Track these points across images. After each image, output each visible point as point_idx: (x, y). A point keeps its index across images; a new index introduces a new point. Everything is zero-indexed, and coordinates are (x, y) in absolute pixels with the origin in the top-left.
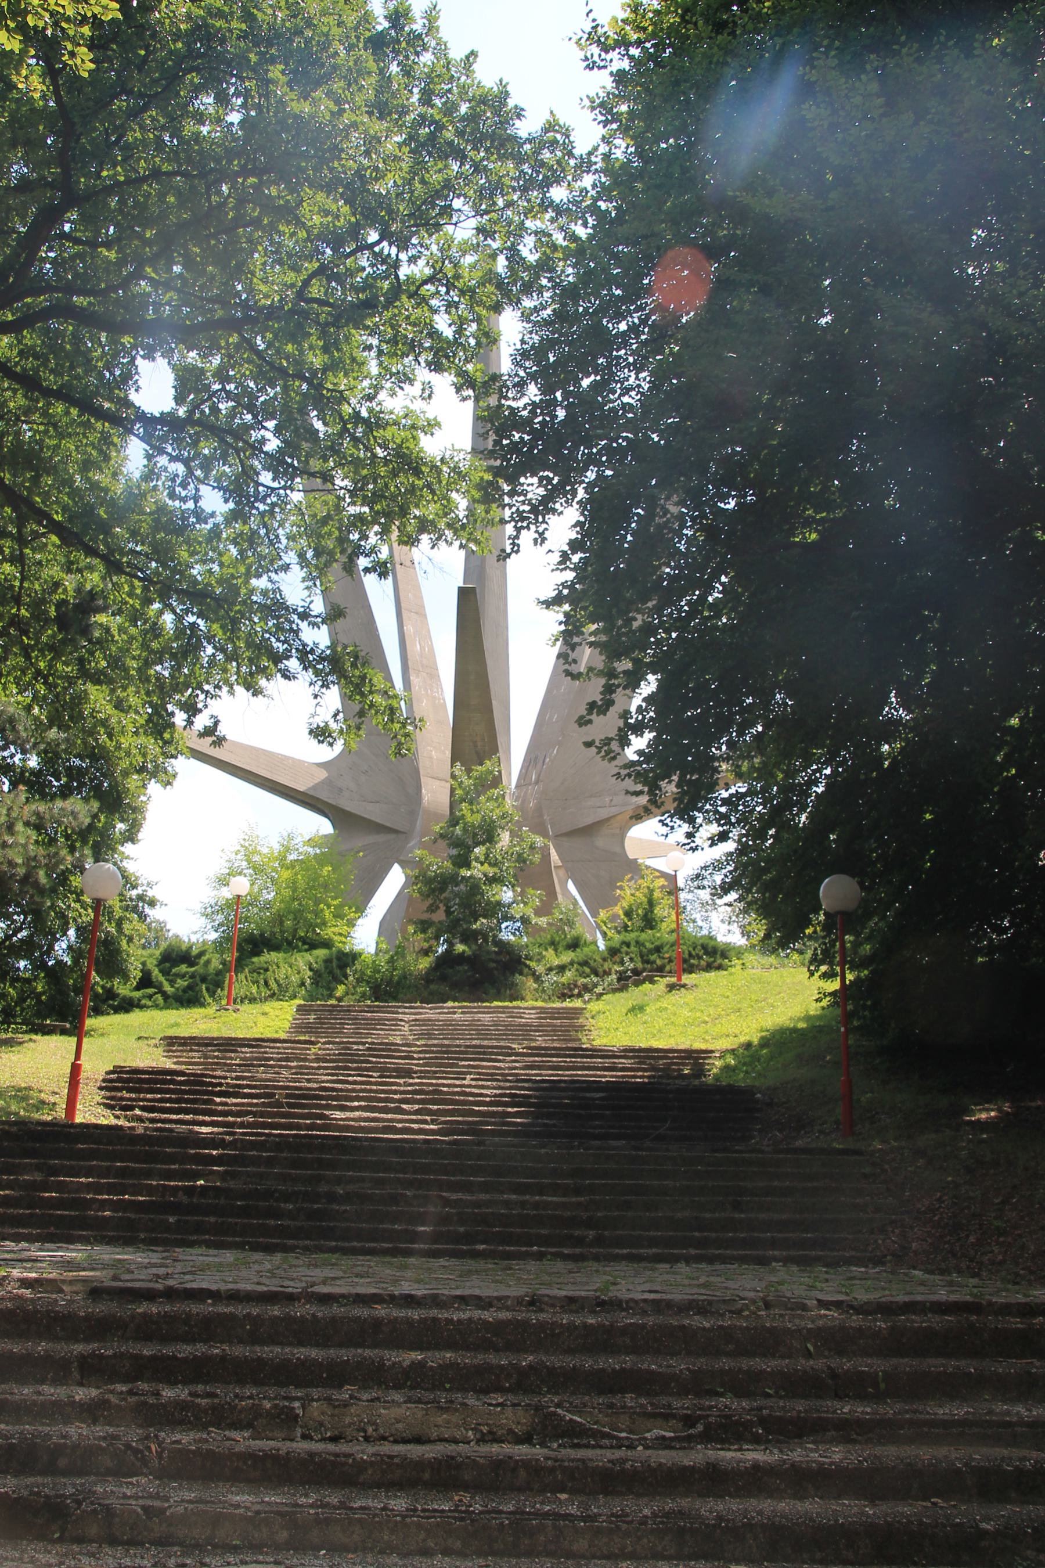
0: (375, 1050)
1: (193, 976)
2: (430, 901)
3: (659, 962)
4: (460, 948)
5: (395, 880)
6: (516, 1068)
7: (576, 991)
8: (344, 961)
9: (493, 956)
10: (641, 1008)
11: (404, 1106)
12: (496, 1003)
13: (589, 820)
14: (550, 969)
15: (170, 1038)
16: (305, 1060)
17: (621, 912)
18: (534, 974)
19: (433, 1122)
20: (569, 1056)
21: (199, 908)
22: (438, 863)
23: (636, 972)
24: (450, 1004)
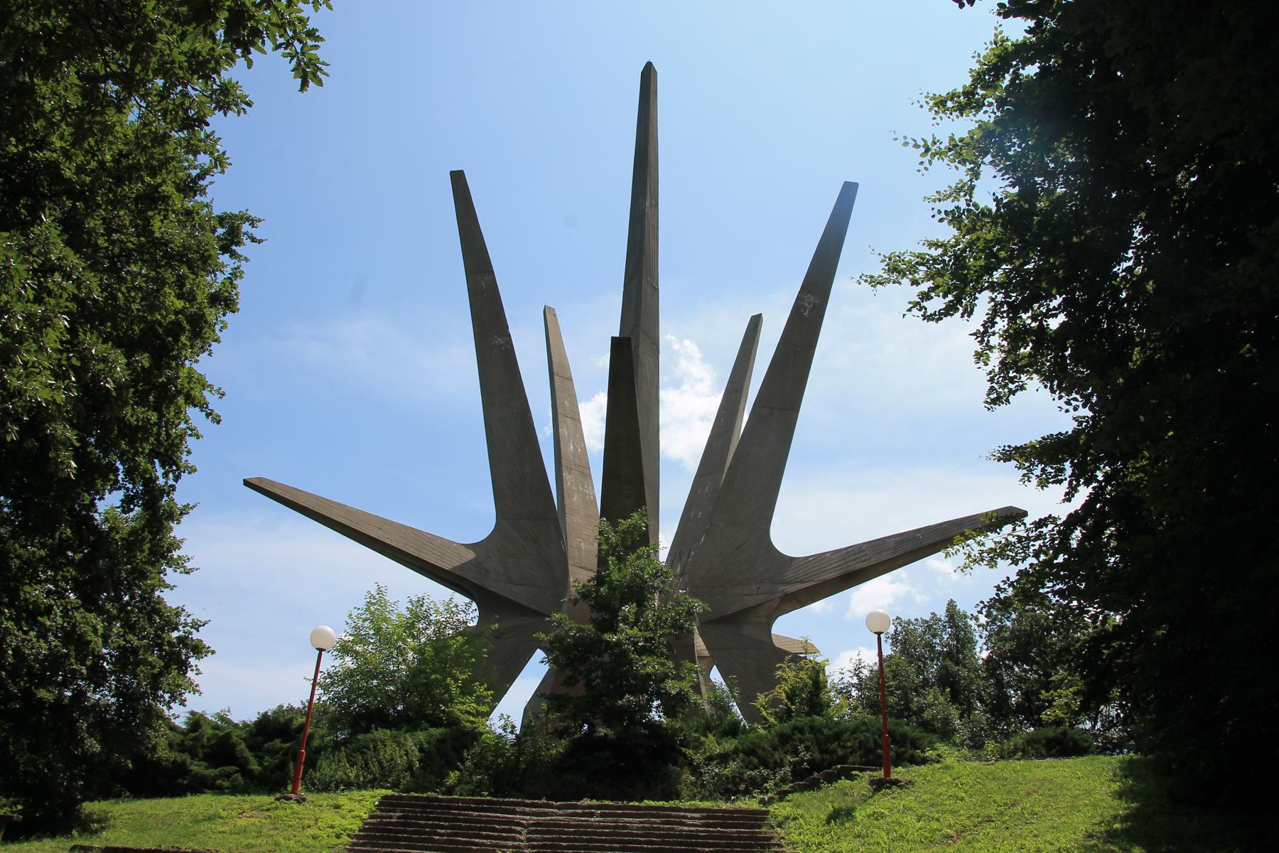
2: (568, 673)
3: (840, 752)
4: (602, 731)
7: (742, 787)
8: (460, 740)
10: (848, 813)
12: (647, 802)
13: (736, 608)
14: (710, 759)
18: (690, 763)
23: (815, 766)
24: (586, 802)
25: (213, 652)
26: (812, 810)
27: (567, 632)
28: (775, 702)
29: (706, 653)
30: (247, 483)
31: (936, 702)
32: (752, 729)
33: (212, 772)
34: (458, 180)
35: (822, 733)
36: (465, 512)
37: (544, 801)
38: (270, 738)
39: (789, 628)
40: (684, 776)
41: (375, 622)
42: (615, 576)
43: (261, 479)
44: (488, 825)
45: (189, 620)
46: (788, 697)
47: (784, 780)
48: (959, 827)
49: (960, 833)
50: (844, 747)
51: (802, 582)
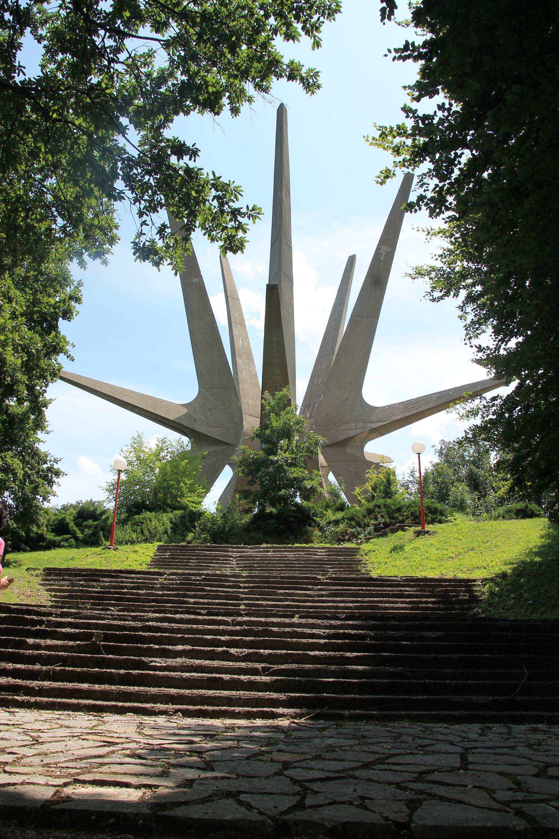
0: (209, 580)
1: (96, 527)
2: (250, 478)
3: (400, 518)
4: (269, 510)
5: (226, 475)
6: (323, 596)
7: (347, 537)
8: (192, 518)
9: (292, 514)
10: (402, 548)
11: (233, 651)
12: (296, 545)
13: (343, 437)
15: (50, 569)
16: (153, 588)
17: (370, 488)
18: (319, 525)
19: (265, 671)
20: (364, 585)
21: (105, 486)
22: (255, 451)
23: (386, 525)
24: (264, 545)
25: (66, 475)
26: (383, 548)
27: (248, 455)
28: (365, 492)
29: (326, 464)
31: (461, 490)
32: (352, 507)
33: (58, 538)
36: (180, 387)
37: (242, 545)
38: (86, 519)
39: (374, 448)
40: (315, 533)
42: (275, 424)
44: (215, 557)
45: (52, 459)
46: (372, 489)
47: (369, 534)
48: (458, 553)
49: (457, 556)
50: (403, 515)
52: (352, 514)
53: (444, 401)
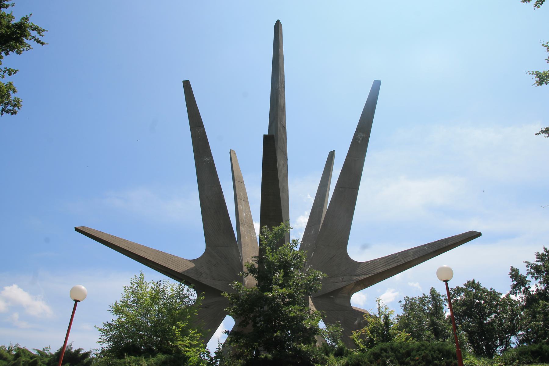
5: (229, 322)
30: (77, 229)
34: (187, 85)
35: (399, 352)
36: (190, 244)
39: (359, 300)
41: (143, 301)
43: (84, 227)
50: (413, 360)
51: (365, 274)
52: (357, 359)
53: (421, 255)
